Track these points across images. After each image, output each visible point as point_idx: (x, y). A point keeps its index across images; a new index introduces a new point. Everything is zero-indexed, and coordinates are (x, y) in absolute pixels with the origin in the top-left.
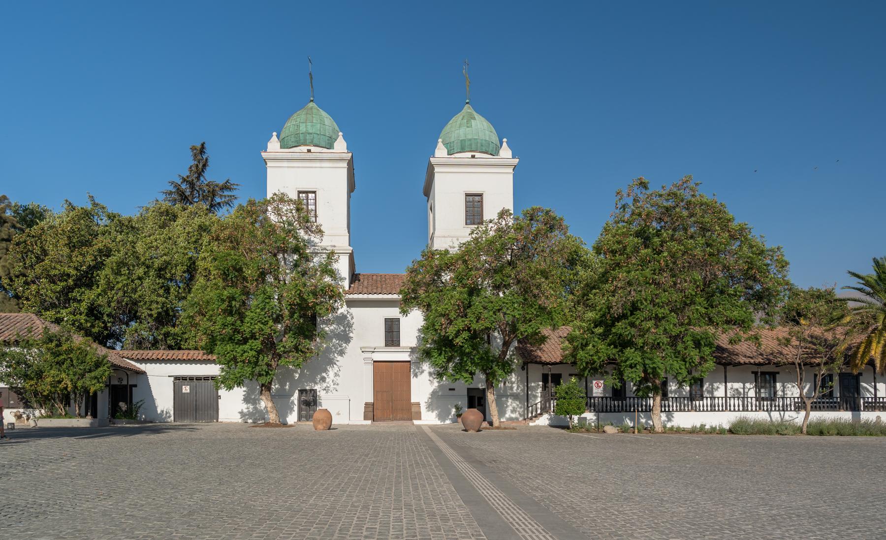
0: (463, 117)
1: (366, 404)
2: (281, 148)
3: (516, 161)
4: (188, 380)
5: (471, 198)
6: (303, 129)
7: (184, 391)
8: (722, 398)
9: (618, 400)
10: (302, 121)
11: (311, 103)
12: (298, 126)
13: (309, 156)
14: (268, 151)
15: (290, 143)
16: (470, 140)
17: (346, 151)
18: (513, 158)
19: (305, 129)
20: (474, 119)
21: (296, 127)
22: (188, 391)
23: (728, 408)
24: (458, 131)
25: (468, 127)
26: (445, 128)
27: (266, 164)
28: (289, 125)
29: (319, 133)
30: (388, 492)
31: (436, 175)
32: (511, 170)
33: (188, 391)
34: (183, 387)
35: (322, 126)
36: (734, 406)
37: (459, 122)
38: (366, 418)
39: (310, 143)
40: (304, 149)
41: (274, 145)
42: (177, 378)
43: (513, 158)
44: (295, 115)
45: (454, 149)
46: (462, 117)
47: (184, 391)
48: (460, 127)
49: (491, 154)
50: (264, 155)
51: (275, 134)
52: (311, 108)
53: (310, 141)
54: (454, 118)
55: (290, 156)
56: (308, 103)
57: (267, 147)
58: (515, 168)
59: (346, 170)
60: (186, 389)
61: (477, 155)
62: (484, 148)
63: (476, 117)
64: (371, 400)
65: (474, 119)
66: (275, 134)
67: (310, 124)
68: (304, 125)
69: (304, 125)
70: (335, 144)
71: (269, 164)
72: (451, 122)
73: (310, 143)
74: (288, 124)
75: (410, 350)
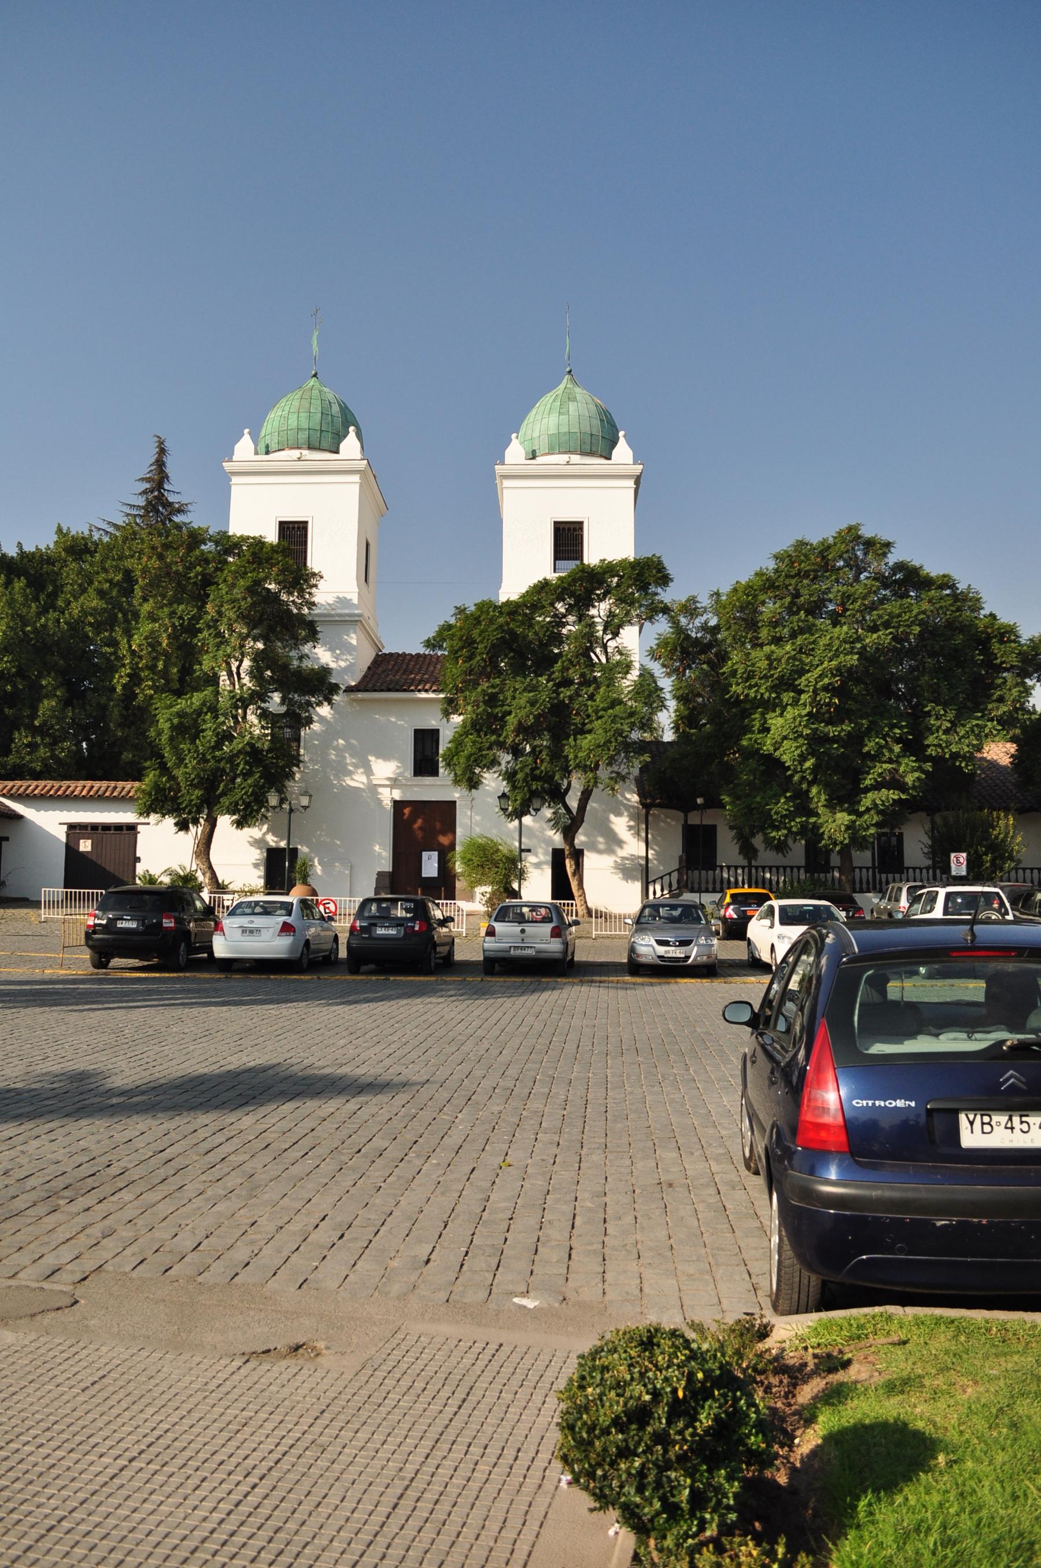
1: (380, 874)
4: (100, 831)
7: (89, 842)
8: (868, 868)
9: (887, 873)
14: (235, 458)
17: (359, 456)
22: (89, 849)
23: (878, 886)
31: (233, 487)
32: (356, 478)
33: (89, 849)
34: (953, 855)
36: (707, 882)
37: (549, 406)
41: (244, 449)
42: (71, 827)
47: (89, 842)
49: (601, 456)
51: (246, 431)
58: (638, 480)
59: (357, 487)
60: (85, 846)
66: (246, 431)
69: (296, 416)
70: (342, 446)
71: (235, 480)
74: (272, 415)
75: (388, 783)
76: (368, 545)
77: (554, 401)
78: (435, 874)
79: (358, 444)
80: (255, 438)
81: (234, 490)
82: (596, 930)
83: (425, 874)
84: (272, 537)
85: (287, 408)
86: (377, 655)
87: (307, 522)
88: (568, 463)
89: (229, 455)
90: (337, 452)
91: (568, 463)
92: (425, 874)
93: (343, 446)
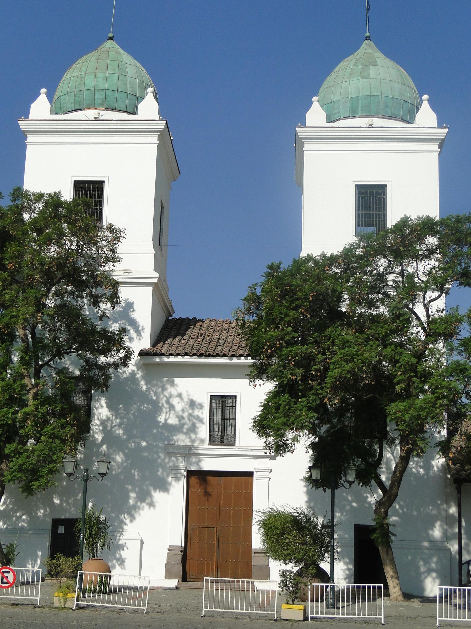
0: (357, 60)
2: (51, 113)
3: (158, 142)
5: (172, 552)
6: (90, 82)
10: (89, 71)
11: (110, 41)
12: (83, 79)
13: (371, 132)
14: (30, 117)
15: (69, 105)
16: (367, 97)
17: (157, 117)
18: (440, 125)
19: (93, 83)
20: (375, 64)
21: (79, 80)
24: (347, 83)
25: (363, 77)
26: (328, 78)
27: (26, 138)
28: (69, 76)
29: (115, 89)
30: (248, 587)
31: (306, 154)
32: (435, 147)
35: (121, 77)
37: (349, 70)
38: (169, 574)
39: (101, 104)
40: (91, 113)
43: (440, 125)
44: (80, 61)
45: (339, 112)
46: (354, 61)
48: (350, 78)
49: (404, 120)
50: (23, 124)
51: (43, 90)
52: (108, 51)
53: (100, 102)
54: (342, 63)
55: (62, 125)
56: (105, 42)
57: (28, 112)
59: (155, 147)
61: (378, 122)
62: (390, 111)
63: (379, 61)
64: (179, 541)
65: (375, 64)
66: (43, 90)
67: (101, 75)
68: (93, 76)
69: (93, 76)
70: (140, 106)
71: (31, 138)
72: (337, 69)
73: (101, 104)
76: (162, 207)
77: (355, 65)
78: (63, 532)
79: (50, 106)
80: (50, 97)
81: (30, 149)
82: (441, 616)
83: (59, 532)
84: (68, 195)
85: (84, 69)
86: (167, 319)
87: (103, 182)
88: (371, 126)
89: (26, 115)
90: (133, 112)
91: (371, 126)
92: (59, 532)
93: (141, 106)
